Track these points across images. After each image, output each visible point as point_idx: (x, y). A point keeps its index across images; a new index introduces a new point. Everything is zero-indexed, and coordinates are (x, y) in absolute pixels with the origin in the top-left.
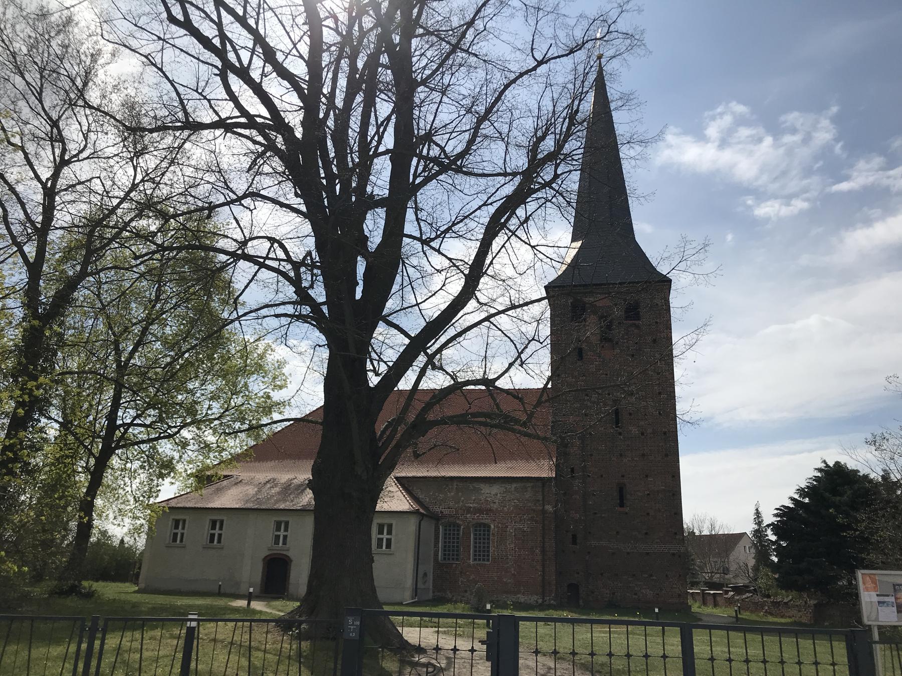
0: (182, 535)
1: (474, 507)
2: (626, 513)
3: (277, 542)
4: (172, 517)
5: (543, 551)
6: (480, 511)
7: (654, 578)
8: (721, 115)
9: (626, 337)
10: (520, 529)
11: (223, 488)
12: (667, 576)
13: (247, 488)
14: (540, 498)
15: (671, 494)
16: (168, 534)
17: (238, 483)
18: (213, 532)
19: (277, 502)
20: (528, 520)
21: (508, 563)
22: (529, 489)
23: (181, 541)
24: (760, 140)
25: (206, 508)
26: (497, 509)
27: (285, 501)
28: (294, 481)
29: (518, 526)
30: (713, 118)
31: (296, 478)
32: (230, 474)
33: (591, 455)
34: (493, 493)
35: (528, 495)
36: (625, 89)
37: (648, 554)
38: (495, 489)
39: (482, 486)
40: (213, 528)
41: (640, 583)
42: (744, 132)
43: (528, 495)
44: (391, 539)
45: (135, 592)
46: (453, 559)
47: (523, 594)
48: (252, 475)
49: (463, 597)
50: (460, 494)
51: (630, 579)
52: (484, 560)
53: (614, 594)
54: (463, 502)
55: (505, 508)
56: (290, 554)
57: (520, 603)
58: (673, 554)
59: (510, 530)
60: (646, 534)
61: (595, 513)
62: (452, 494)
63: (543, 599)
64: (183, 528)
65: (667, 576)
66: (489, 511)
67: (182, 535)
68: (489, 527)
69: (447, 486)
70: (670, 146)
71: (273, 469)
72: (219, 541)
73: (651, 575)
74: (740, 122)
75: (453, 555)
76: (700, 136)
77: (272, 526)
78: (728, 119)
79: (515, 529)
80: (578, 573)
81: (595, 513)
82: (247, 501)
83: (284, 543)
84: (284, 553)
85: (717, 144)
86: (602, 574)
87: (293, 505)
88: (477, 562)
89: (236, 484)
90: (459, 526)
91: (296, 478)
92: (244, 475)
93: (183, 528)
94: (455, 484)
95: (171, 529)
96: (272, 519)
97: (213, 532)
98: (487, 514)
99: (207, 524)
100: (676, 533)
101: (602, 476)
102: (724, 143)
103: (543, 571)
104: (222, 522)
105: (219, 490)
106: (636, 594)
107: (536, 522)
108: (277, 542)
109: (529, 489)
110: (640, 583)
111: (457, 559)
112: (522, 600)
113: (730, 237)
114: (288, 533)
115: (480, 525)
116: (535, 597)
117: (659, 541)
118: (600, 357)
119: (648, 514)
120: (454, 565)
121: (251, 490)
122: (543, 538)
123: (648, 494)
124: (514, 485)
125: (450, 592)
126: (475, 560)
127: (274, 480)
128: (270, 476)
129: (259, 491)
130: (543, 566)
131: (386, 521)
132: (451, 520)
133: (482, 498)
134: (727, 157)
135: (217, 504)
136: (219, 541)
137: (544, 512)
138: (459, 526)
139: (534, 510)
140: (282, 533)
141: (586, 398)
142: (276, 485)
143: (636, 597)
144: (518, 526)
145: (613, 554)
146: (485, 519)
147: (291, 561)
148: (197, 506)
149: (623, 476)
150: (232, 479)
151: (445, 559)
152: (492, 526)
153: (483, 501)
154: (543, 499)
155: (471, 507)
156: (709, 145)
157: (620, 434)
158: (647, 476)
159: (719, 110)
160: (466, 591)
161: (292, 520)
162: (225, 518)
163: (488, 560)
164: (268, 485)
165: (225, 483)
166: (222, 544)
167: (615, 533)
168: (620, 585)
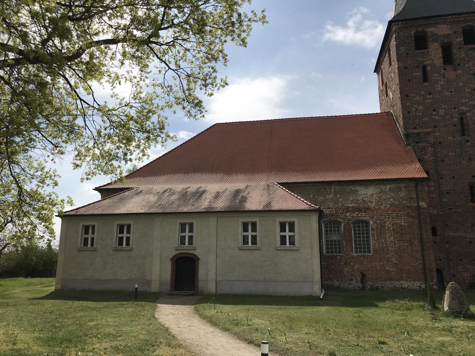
0: (93, 239)
1: (353, 207)
3: (183, 243)
4: (82, 224)
5: (422, 242)
6: (358, 209)
8: (355, 14)
9: (467, 59)
10: (398, 224)
11: (126, 197)
13: (148, 196)
14: (414, 196)
16: (80, 239)
17: (139, 193)
18: (121, 235)
19: (179, 206)
20: (405, 216)
21: (389, 254)
22: (403, 189)
23: (92, 245)
24: (376, 27)
25: (113, 214)
26: (374, 207)
27: (186, 205)
28: (189, 190)
29: (395, 221)
30: (351, 16)
31: (189, 187)
32: (130, 186)
33: (443, 160)
35: (402, 194)
38: (371, 190)
39: (358, 188)
40: (121, 232)
42: (368, 23)
43: (402, 194)
44: (256, 236)
45: (52, 296)
46: (336, 252)
47: (406, 280)
48: (150, 186)
49: (350, 284)
50: (338, 196)
52: (364, 252)
54: (341, 203)
55: (382, 207)
56: (197, 253)
57: (404, 289)
59: (388, 224)
61: (451, 209)
62: (331, 196)
64: (93, 233)
66: (367, 209)
67: (93, 239)
69: (325, 189)
70: (329, 32)
71: (166, 182)
72: (128, 244)
74: (366, 17)
75: (336, 248)
76: (345, 26)
77: (178, 227)
78: (359, 17)
79: (393, 224)
80: (440, 260)
81: (451, 209)
82: (151, 207)
83: (191, 243)
84: (191, 252)
85: (353, 29)
86: (461, 260)
87: (196, 208)
88: (359, 254)
89: (137, 194)
90: (339, 223)
91: (189, 187)
92: (143, 187)
93: (93, 233)
94: (333, 187)
95: (117, 235)
96: (176, 224)
97: (121, 235)
98: (365, 212)
99: (115, 229)
101: (454, 177)
102: (358, 29)
103: (423, 260)
104: (129, 227)
105: (122, 199)
107: (413, 217)
108: (183, 243)
109: (403, 189)
111: (340, 252)
112: (406, 286)
113: (363, 79)
114: (131, 235)
115: (363, 222)
116: (418, 283)
118: (444, 77)
120: (339, 258)
121: (153, 198)
122: (421, 230)
124: (388, 187)
125: (338, 281)
126: (356, 252)
127: (171, 190)
128: (166, 186)
129: (160, 198)
130: (423, 255)
131: (287, 219)
132: (332, 218)
133: (360, 198)
134: (359, 36)
135: (123, 210)
136: (128, 244)
137: (419, 207)
138: (339, 223)
139: (410, 207)
140: (125, 235)
141: (434, 113)
142: (173, 194)
144: (395, 221)
146: (363, 216)
147: (198, 259)
148: (104, 213)
150: (133, 190)
151: (328, 252)
152: (371, 222)
153: (361, 201)
154: (417, 197)
155: (349, 207)
156: (350, 30)
157: (468, 141)
159: (354, 11)
160: (352, 280)
161: (196, 222)
162: (132, 223)
163: (369, 252)
164: (167, 194)
165: (127, 193)
166: (131, 246)
167: (470, 225)
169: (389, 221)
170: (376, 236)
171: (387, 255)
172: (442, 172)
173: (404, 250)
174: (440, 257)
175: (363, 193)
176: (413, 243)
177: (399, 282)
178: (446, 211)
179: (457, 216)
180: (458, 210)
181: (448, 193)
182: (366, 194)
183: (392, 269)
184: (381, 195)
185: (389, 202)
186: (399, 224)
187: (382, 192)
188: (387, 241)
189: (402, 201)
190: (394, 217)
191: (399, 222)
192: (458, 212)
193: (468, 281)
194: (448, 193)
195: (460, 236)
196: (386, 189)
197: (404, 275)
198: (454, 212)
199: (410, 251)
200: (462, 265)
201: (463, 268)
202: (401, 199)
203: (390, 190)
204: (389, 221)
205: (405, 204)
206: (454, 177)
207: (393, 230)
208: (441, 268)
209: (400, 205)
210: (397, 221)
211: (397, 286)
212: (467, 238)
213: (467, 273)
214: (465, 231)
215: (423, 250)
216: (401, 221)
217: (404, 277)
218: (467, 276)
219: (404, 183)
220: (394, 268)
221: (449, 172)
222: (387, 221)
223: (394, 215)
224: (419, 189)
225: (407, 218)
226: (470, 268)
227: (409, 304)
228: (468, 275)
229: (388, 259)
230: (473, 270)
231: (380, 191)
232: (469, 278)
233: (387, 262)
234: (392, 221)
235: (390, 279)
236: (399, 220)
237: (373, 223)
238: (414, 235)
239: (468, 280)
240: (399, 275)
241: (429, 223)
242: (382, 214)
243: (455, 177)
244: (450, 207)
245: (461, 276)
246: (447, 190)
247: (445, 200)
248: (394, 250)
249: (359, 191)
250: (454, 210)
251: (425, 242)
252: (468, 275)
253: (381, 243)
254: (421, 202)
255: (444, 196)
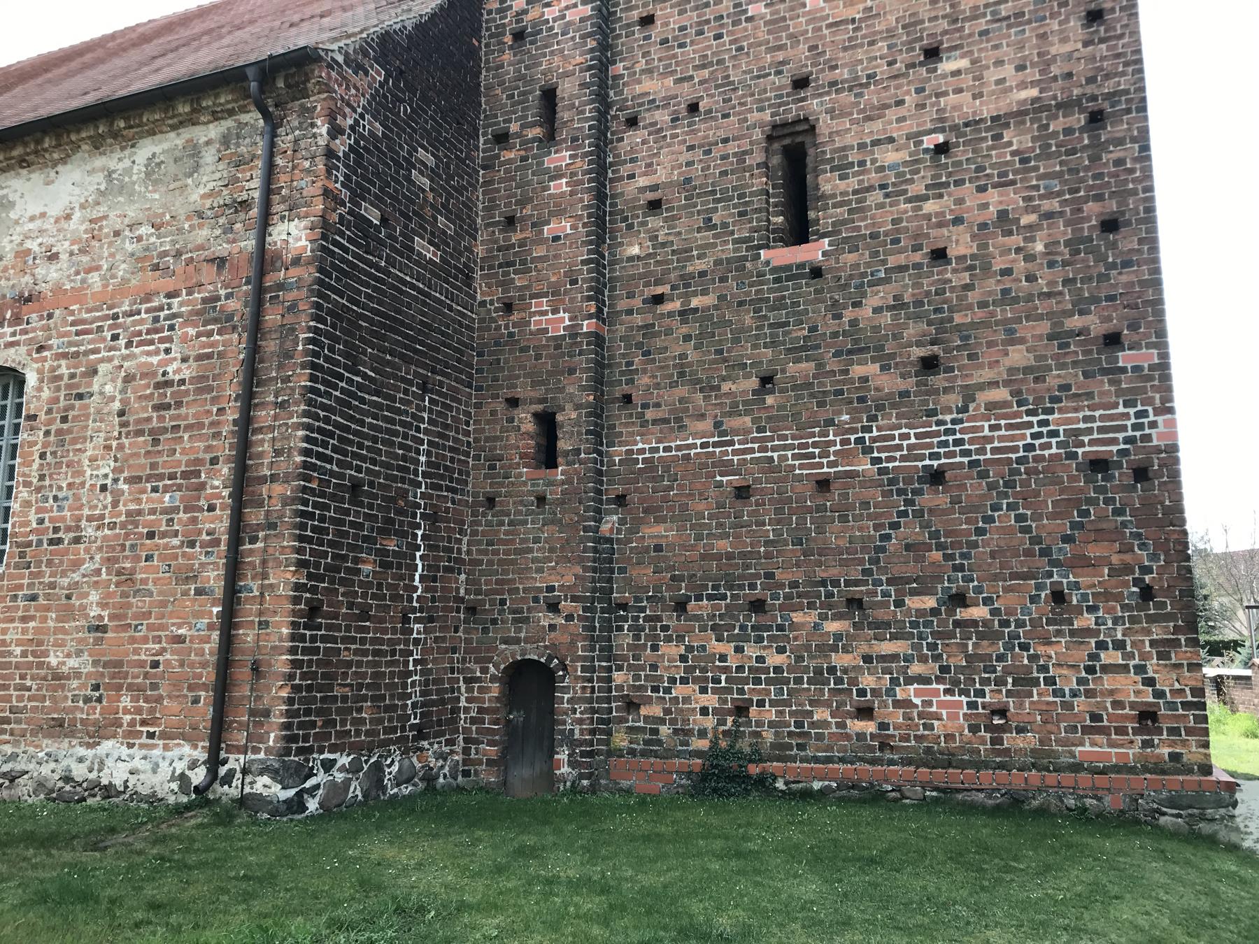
2: (816, 272)
7: (979, 612)
12: (1058, 597)
15: (1079, 119)
22: (209, 156)
33: (647, 21)
34: (55, 210)
36: (1201, 533)
37: (936, 477)
41: (887, 647)
51: (832, 627)
53: (741, 710)
55: (94, 278)
58: (1099, 465)
59: (105, 385)
60: (929, 365)
61: (658, 299)
63: (214, 762)
65: (1058, 597)
68: (21, 381)
73: (960, 600)
79: (128, 379)
80: (553, 607)
81: (658, 299)
86: (681, 606)
100: (1113, 340)
101: (693, 108)
106: (865, 712)
110: (887, 647)
117: (1002, 394)
119: (939, 255)
123: (942, 149)
137: (264, 260)
143: (870, 727)
145: (742, 493)
149: (801, 83)
158: (933, 54)
167: (754, 383)
168: (774, 659)
169: (110, 360)
170: (36, 456)
171: (64, 574)
172: (638, 89)
173: (151, 535)
174: (551, 589)
175: (29, 214)
176: (202, 486)
177: (89, 746)
178: (630, 312)
179: (687, 338)
180: (695, 302)
181: (655, 206)
182: (43, 215)
183: (73, 663)
184: (103, 209)
185: (130, 247)
186: (154, 374)
187: (114, 186)
188: (83, 484)
189: (192, 227)
190: (139, 333)
191: (155, 360)
192: (696, 310)
193: (703, 744)
194: (655, 206)
195: (687, 457)
196: (128, 171)
197: (126, 701)
198: (670, 314)
199: (176, 542)
200: (680, 639)
201: (683, 658)
202: (188, 218)
203: (148, 174)
204: (110, 360)
205: (201, 248)
206: (693, 108)
207: (121, 413)
208: (550, 659)
209: (178, 254)
210: (148, 354)
211: (79, 772)
212: (726, 468)
213: (704, 690)
214: (717, 425)
215: (238, 531)
216: (167, 351)
217: (126, 711)
218: (704, 711)
219: (216, 117)
220: (86, 656)
221: (670, 81)
222: (102, 360)
223: (142, 322)
224: (285, 141)
225: (199, 335)
226: (723, 658)
227: (530, 840)
228: (711, 700)
229: (68, 597)
230: (740, 669)
231: (103, 188)
232: (710, 722)
233: (58, 620)
234: (125, 358)
235: (59, 728)
236: (157, 352)
237: (41, 380)
238: (217, 435)
239: (702, 733)
240: (99, 700)
241: (306, 352)
242: (83, 322)
243: (703, 106)
244: (659, 290)
245: (667, 711)
246: (654, 188)
247: (635, 250)
248: (105, 538)
249: (12, 204)
250: (676, 305)
251: (263, 480)
252: (711, 700)
253: (56, 498)
254: (282, 218)
255: (630, 227)
